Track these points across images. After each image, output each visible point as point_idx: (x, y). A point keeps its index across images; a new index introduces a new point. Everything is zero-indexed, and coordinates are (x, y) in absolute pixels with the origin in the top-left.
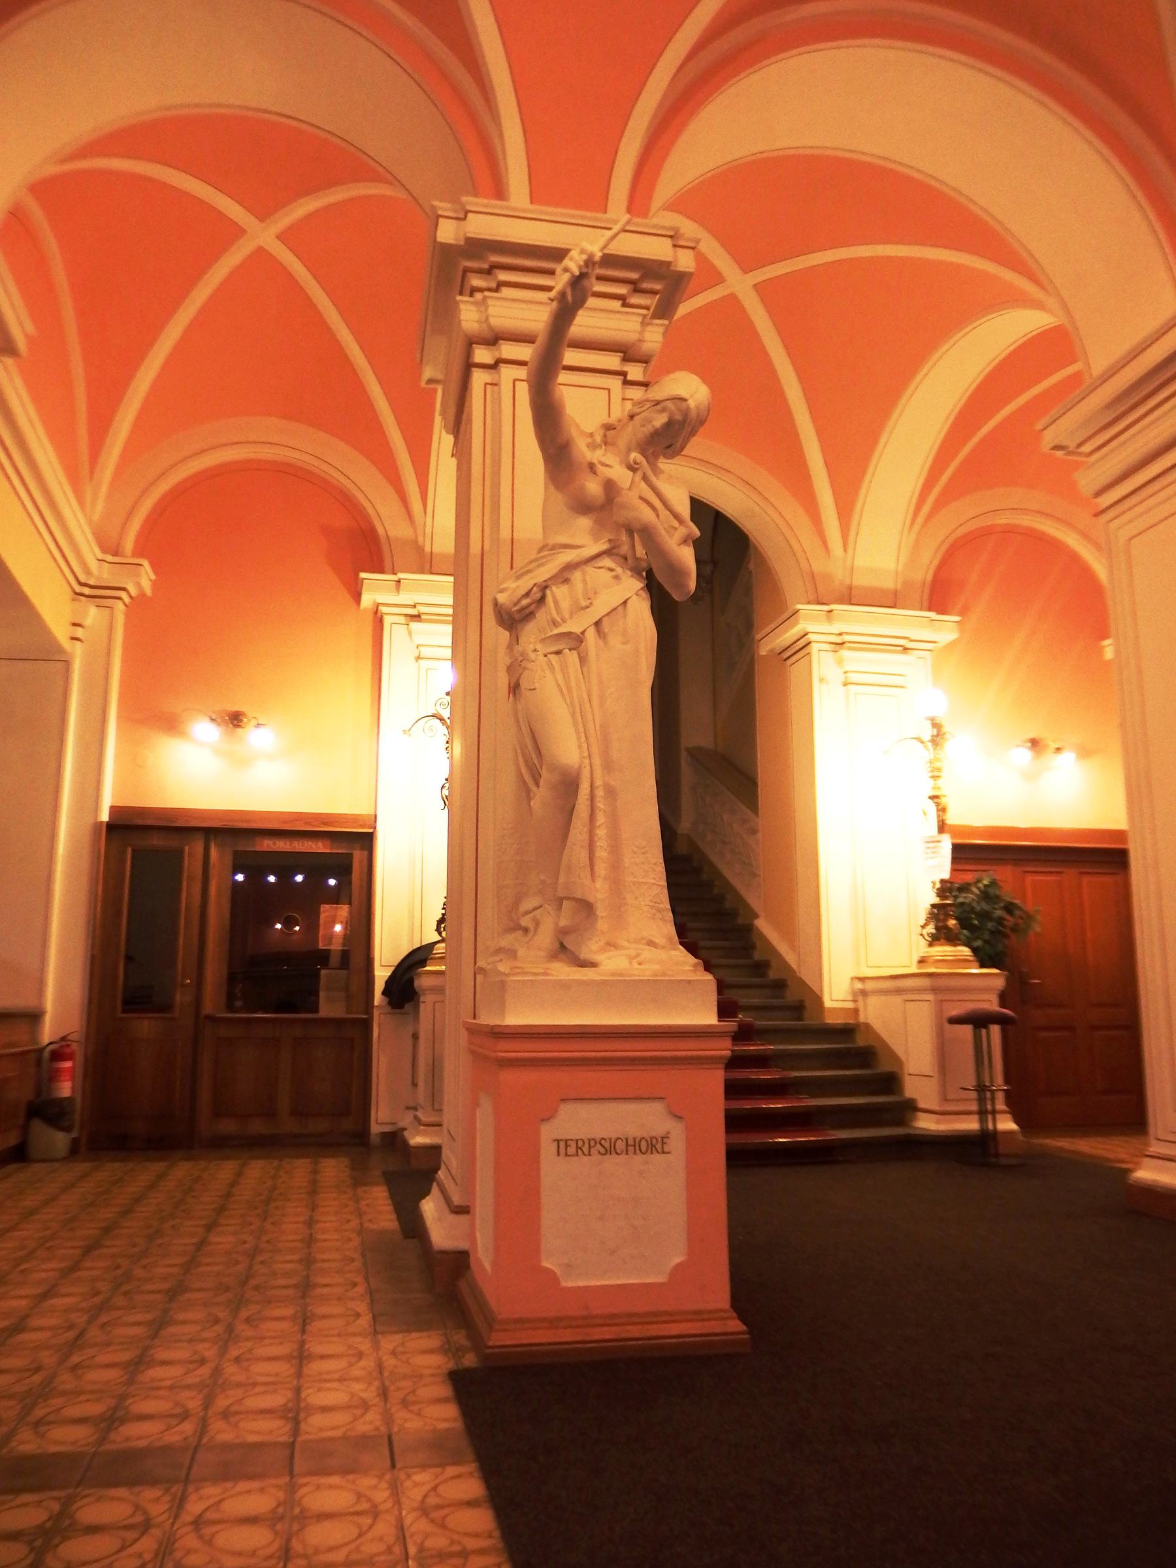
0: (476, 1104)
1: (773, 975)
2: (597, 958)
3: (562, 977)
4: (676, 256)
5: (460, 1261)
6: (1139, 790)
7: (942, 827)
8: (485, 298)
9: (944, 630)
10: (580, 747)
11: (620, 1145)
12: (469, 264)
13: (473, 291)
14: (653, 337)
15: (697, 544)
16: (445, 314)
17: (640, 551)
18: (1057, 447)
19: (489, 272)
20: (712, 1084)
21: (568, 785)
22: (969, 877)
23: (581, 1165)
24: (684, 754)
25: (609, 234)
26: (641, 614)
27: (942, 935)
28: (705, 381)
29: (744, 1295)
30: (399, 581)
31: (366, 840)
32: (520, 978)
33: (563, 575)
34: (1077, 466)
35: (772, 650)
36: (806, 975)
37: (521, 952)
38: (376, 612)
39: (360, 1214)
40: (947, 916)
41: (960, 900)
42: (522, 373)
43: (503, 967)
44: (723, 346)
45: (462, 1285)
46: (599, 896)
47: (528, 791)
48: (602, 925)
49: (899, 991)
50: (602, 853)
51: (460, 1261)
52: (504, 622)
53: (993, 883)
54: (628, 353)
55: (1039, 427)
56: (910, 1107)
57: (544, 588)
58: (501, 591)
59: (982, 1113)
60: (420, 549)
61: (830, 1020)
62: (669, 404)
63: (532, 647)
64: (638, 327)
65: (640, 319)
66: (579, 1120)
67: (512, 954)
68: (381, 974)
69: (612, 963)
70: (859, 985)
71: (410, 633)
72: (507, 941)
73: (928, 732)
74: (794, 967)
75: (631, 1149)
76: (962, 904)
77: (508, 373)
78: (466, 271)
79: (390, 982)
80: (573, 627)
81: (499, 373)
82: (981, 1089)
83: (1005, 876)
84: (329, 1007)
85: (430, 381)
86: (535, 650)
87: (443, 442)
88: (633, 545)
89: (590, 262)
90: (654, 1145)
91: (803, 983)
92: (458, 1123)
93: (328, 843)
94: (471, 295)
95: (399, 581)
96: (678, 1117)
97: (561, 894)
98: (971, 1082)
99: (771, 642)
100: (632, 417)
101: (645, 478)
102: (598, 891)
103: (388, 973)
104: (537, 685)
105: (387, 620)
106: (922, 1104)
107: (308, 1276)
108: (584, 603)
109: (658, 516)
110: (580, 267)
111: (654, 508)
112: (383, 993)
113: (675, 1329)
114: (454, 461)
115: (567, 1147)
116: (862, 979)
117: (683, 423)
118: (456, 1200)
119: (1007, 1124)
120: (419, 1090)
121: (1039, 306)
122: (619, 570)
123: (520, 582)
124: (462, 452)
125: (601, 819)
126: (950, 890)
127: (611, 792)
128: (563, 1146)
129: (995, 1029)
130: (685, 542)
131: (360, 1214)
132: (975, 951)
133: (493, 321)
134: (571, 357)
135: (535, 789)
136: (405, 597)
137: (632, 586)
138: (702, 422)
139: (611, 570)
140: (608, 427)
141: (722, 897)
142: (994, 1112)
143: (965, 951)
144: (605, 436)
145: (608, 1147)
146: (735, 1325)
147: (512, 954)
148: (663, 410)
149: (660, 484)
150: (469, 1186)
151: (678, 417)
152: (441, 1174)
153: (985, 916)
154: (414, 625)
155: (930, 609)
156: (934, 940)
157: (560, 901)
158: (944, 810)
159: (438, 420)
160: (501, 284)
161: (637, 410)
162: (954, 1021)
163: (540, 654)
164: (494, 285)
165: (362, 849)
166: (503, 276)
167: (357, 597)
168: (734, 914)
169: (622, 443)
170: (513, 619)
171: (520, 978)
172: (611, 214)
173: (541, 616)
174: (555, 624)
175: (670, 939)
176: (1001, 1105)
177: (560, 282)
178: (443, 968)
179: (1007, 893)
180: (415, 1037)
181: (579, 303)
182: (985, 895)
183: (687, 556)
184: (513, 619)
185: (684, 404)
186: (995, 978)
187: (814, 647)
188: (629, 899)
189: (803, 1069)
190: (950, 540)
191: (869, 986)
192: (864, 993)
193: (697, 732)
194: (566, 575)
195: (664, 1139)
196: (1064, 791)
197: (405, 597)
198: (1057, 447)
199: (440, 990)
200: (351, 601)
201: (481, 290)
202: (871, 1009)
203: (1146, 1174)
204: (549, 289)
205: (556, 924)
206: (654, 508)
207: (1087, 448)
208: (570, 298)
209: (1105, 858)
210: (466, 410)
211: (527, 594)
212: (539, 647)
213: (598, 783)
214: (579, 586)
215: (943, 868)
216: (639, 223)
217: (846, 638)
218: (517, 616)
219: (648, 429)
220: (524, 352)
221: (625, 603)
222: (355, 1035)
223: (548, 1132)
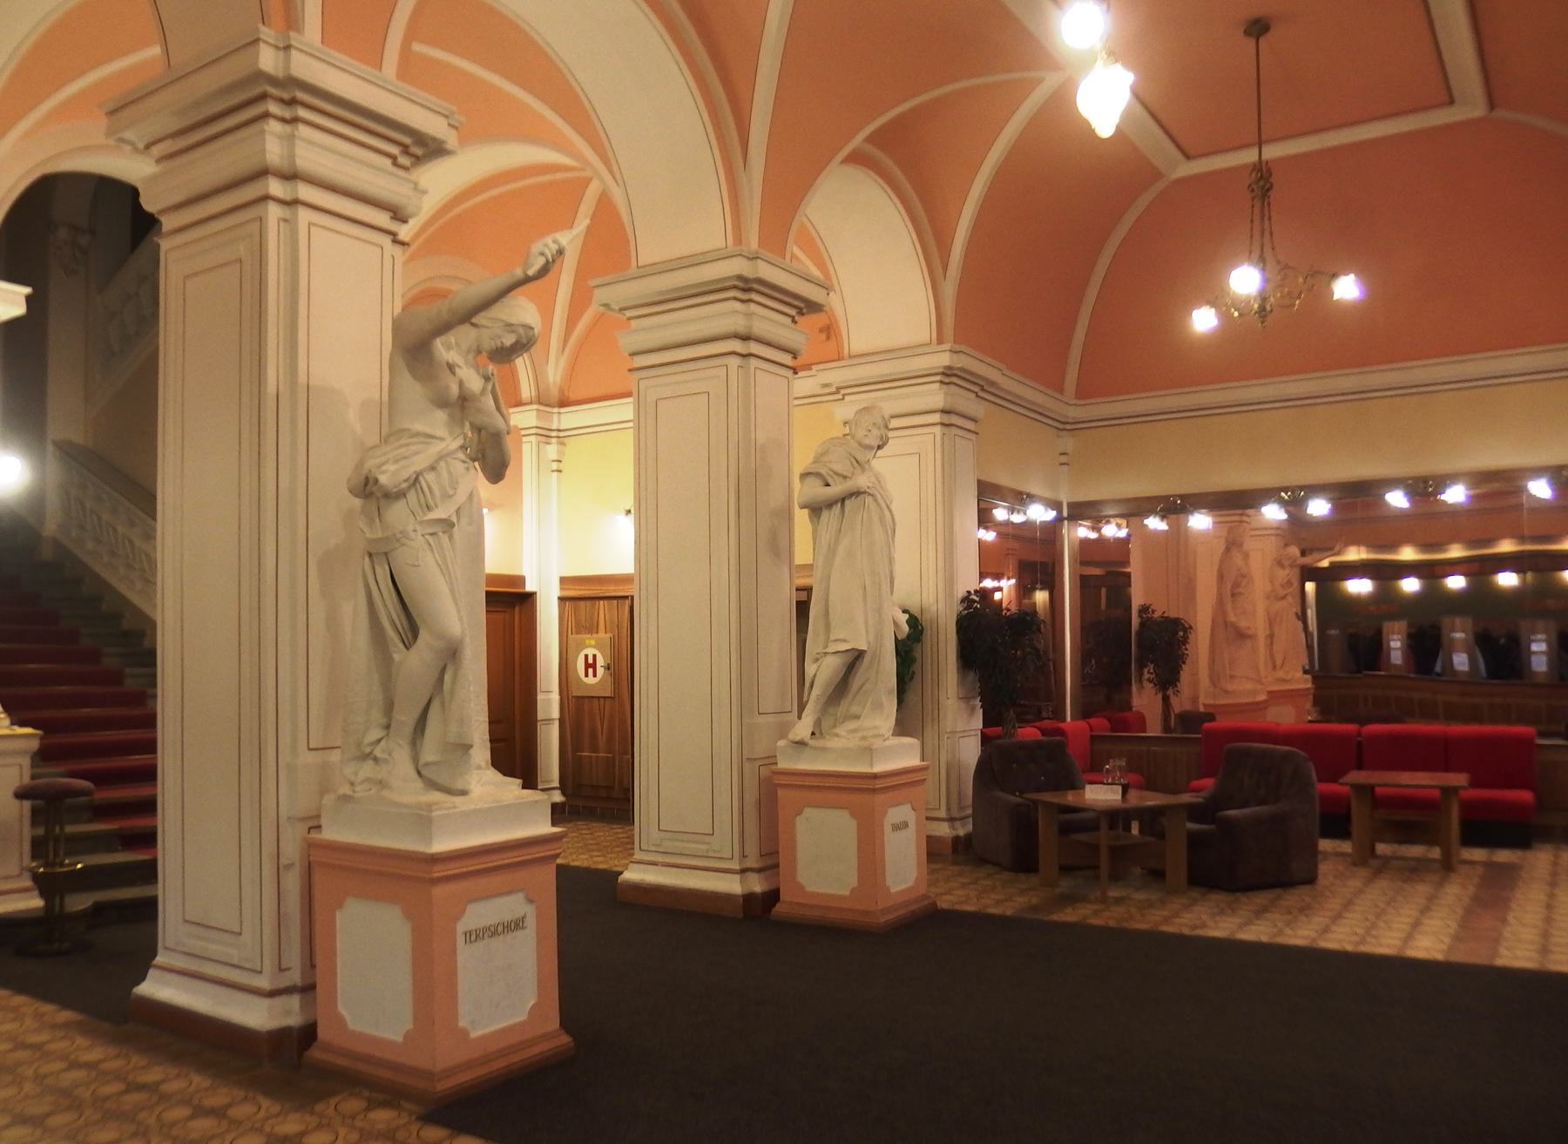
29: (568, 1020)
55: (593, 283)
90: (518, 924)
96: (530, 901)
113: (536, 1050)
115: (474, 936)
146: (565, 1039)
160: (750, 301)
166: (302, 113)
203: (632, 875)
214: (445, 474)
223: (463, 926)
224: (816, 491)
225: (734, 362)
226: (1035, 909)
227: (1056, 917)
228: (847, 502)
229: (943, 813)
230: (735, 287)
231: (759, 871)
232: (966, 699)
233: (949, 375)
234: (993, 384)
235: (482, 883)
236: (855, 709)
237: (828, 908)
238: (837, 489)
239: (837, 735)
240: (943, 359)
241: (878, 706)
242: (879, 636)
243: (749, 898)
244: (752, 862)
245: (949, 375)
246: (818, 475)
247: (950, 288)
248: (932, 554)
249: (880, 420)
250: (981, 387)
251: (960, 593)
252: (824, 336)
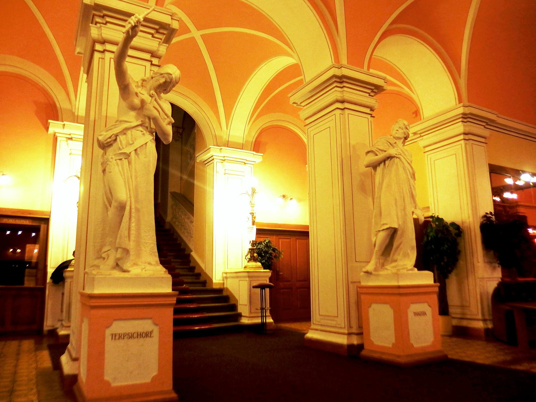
0: (82, 321)
1: (196, 271)
2: (130, 269)
3: (116, 276)
4: (172, 23)
5: (74, 378)
6: (313, 212)
7: (254, 223)
8: (101, 26)
9: (258, 158)
10: (127, 194)
11: (135, 335)
12: (94, 12)
13: (96, 23)
14: (163, 50)
15: (174, 126)
16: (85, 31)
17: (153, 126)
18: (294, 103)
19: (103, 17)
20: (169, 314)
21: (122, 207)
22: (262, 240)
23: (121, 343)
24: (169, 194)
25: (149, 11)
26: (152, 147)
27: (253, 259)
28: (179, 68)
29: (176, 386)
30: (64, 125)
31: (46, 221)
32: (100, 276)
33: (124, 132)
34: (300, 109)
35: (201, 161)
36: (207, 272)
37: (101, 267)
38: (55, 135)
39: (36, 361)
40: (254, 252)
41: (258, 247)
42: (112, 55)
43: (94, 272)
44: (188, 57)
45: (75, 388)
46: (131, 247)
47: (107, 208)
48: (132, 257)
49: (237, 277)
50: (133, 232)
51: (74, 378)
52: (102, 146)
53: (269, 242)
54: (153, 54)
55: (289, 95)
56: (240, 315)
57: (116, 136)
58: (101, 135)
59: (262, 317)
60: (73, 114)
61: (215, 287)
62: (166, 75)
63: (111, 157)
64: (157, 46)
65: (158, 43)
66: (120, 327)
67: (98, 267)
68: (50, 271)
69: (135, 271)
70: (225, 275)
71: (68, 144)
72: (96, 262)
73: (250, 192)
74: (204, 269)
75: (139, 336)
76: (259, 248)
77: (108, 55)
78: (94, 15)
79: (53, 274)
80: (127, 150)
81: (105, 54)
82: (262, 309)
83: (273, 240)
84: (29, 283)
85: (79, 53)
86: (112, 158)
87: (83, 76)
88: (150, 124)
89: (138, 22)
91: (205, 274)
92: (76, 328)
93: (31, 221)
94: (96, 24)
95: (64, 125)
96: (156, 325)
97: (117, 246)
98: (259, 307)
99: (201, 157)
100: (152, 78)
101: (156, 100)
102: (131, 246)
103: (53, 270)
104: (112, 171)
105: (59, 139)
106: (243, 314)
107: (13, 387)
108: (131, 142)
109: (159, 114)
110: (135, 23)
111: (158, 111)
112: (51, 278)
114: (86, 84)
116: (226, 273)
117: (170, 82)
118: (74, 355)
119: (270, 320)
120: (64, 315)
121: (291, 56)
122: (145, 132)
123: (108, 133)
124: (89, 81)
125: (133, 220)
126: (256, 244)
127: (138, 210)
128: (114, 336)
129: (267, 290)
130: (169, 124)
131: (36, 361)
132: (262, 264)
133: (104, 35)
134: (130, 52)
135: (109, 207)
136: (67, 131)
137: (149, 140)
138: (177, 83)
139: (142, 131)
140: (144, 80)
141: (175, 248)
142: (266, 316)
143: (259, 264)
144: (142, 83)
145: (131, 336)
146: (174, 395)
147: (98, 267)
148: (163, 77)
149: (160, 102)
150: (79, 350)
151: (169, 80)
152: (69, 346)
153: (266, 252)
154: (69, 141)
155: (253, 151)
156: (250, 260)
157: (117, 249)
158: (255, 218)
159: (82, 69)
160: (344, 87)
161: (154, 76)
162: (254, 287)
163: (114, 159)
164: (104, 22)
165: (45, 224)
166: (108, 19)
167: (47, 129)
168: (184, 250)
169: (148, 87)
170: (105, 146)
171: (100, 276)
172: (149, 4)
173: (115, 145)
174: (120, 149)
175: (157, 262)
176: (268, 314)
177: (128, 26)
178: (73, 269)
179: (273, 245)
180: (63, 294)
181: (134, 35)
182: (267, 246)
183: (169, 129)
184: (105, 146)
185: (171, 76)
186: (268, 273)
187: (215, 161)
188: (143, 248)
189: (206, 303)
190: (261, 129)
191: (228, 275)
192: (226, 278)
193: (173, 187)
194: (125, 132)
195: (151, 332)
196: (291, 213)
197: (67, 131)
198: (294, 103)
199: (72, 277)
200: (45, 131)
201: (100, 23)
202: (228, 282)
203: (311, 335)
204: (124, 26)
205: (115, 256)
206: (158, 111)
207: (303, 104)
208: (130, 33)
209: (302, 234)
210: (91, 66)
211: (110, 138)
212: (113, 157)
213: (133, 207)
215: (253, 237)
216: (158, 8)
217: (225, 158)
218: (106, 145)
219: (158, 83)
220: (114, 48)
221: (146, 143)
222: (38, 296)
223: (108, 332)
224: (372, 158)
225: (338, 112)
226: (504, 362)
227: (513, 367)
228: (387, 162)
229: (480, 317)
230: (336, 81)
231: (357, 334)
232: (490, 263)
233: (465, 117)
234: (493, 121)
235: (123, 311)
236: (396, 257)
237: (383, 353)
238: (381, 156)
239: (387, 269)
240: (461, 110)
241: (406, 255)
242: (405, 222)
243: (351, 347)
244: (354, 330)
245: (465, 117)
246: (372, 151)
247: (463, 82)
248: (465, 196)
249: (402, 126)
250: (488, 123)
251: (482, 213)
252: (414, 115)
